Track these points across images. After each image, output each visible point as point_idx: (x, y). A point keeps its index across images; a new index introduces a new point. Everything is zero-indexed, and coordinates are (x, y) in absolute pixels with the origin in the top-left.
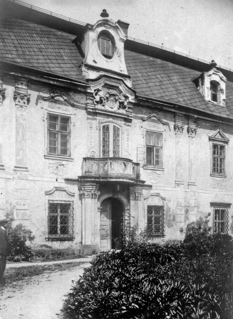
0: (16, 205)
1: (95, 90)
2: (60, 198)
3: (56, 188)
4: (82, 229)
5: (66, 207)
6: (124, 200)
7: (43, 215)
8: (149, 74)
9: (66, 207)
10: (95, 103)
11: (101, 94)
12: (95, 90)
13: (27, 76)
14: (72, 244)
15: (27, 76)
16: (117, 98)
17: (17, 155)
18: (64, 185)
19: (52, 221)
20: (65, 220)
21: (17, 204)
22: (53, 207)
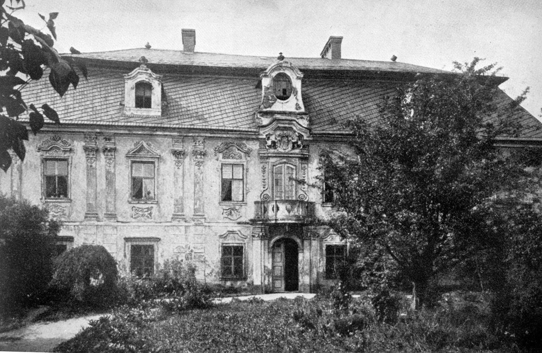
0: (193, 249)
1: (266, 135)
2: (232, 242)
3: (229, 231)
4: (21, 179)
5: (239, 251)
6: (299, 241)
7: (215, 257)
8: (236, 117)
9: (239, 251)
10: (267, 148)
11: (273, 138)
12: (266, 135)
13: (202, 135)
14: (184, 259)
15: (202, 135)
16: (290, 138)
17: (195, 204)
18: (236, 228)
19: (225, 262)
20: (239, 262)
21: (194, 248)
22: (226, 250)
